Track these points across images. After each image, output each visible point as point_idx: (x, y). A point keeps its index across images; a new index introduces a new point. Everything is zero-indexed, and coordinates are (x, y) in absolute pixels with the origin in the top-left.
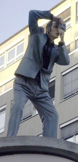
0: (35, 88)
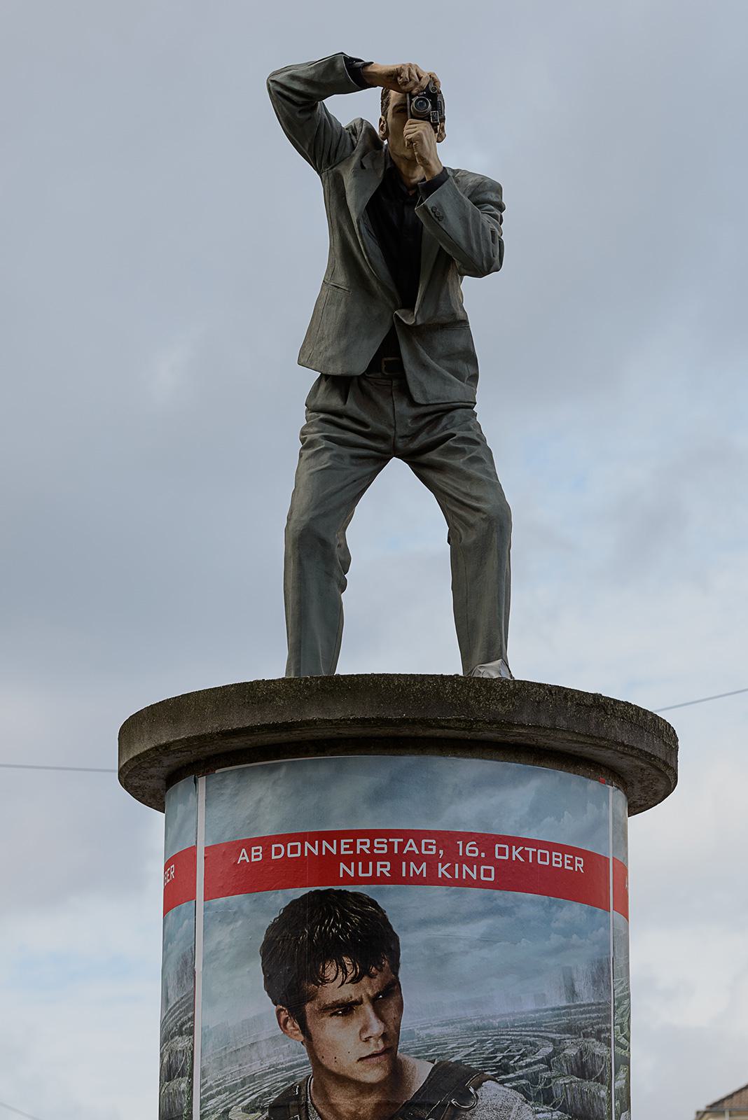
0: (389, 410)
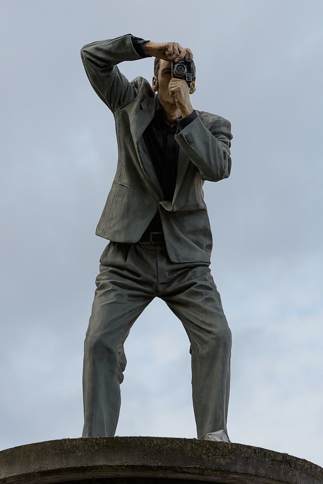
0: (154, 265)
